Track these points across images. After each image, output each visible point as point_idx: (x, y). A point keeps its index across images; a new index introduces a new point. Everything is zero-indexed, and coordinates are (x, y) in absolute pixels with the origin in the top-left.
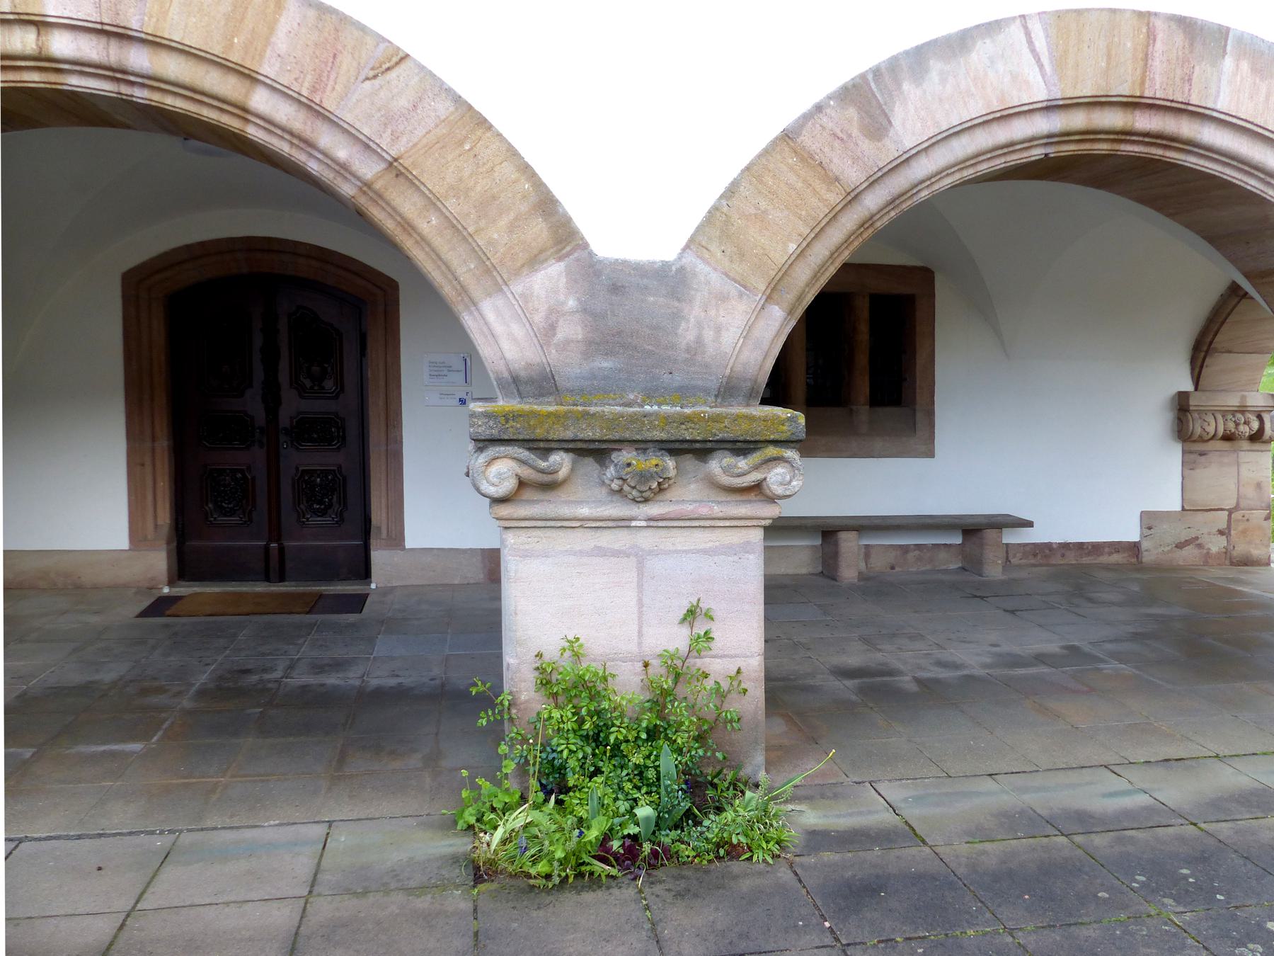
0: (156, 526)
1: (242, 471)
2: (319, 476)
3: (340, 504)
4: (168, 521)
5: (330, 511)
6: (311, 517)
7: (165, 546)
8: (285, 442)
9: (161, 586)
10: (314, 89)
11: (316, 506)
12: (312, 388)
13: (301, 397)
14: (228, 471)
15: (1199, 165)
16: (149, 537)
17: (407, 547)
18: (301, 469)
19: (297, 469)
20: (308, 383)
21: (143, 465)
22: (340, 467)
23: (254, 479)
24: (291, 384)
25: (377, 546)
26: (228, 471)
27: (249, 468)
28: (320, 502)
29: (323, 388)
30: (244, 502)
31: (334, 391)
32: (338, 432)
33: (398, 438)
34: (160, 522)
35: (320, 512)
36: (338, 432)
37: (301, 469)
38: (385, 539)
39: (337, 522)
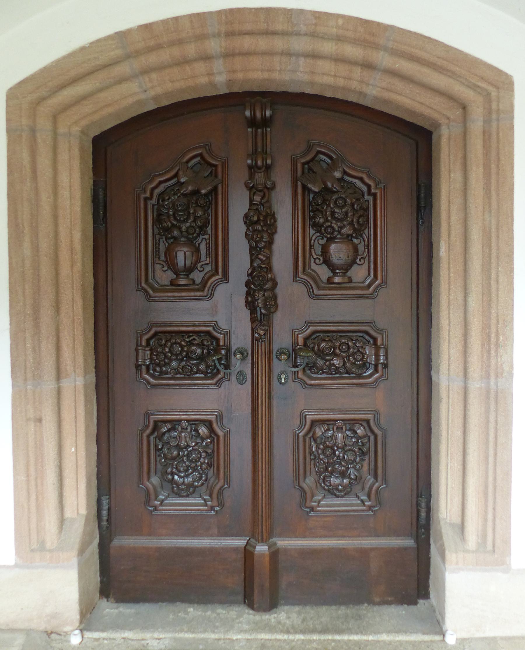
0: (62, 521)
1: (209, 424)
2: (340, 429)
3: (376, 477)
4: (83, 511)
5: (357, 488)
6: (324, 497)
7: (75, 561)
8: (283, 384)
9: (67, 629)
10: (256, 132)
11: (334, 481)
12: (329, 280)
13: (313, 296)
14: (184, 424)
15: (449, 218)
16: (48, 545)
17: (247, 289)
18: (309, 418)
19: (303, 418)
20: (324, 272)
21: (40, 420)
22: (377, 414)
23: (227, 434)
24: (296, 274)
25: (457, 563)
26: (184, 424)
27: (220, 417)
28: (343, 475)
29: (350, 280)
30: (210, 473)
31: (369, 286)
32: (377, 356)
33: (506, 368)
34: (69, 513)
35: (339, 491)
36: (377, 356)
37: (309, 418)
38: (473, 552)
39: (370, 508)
